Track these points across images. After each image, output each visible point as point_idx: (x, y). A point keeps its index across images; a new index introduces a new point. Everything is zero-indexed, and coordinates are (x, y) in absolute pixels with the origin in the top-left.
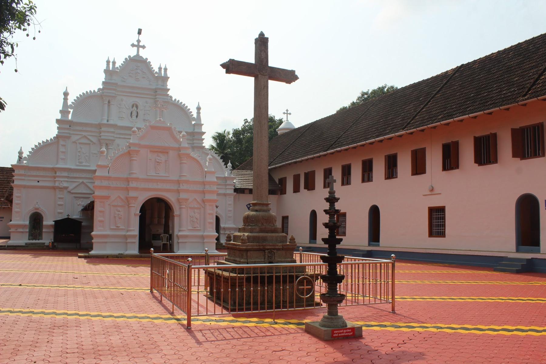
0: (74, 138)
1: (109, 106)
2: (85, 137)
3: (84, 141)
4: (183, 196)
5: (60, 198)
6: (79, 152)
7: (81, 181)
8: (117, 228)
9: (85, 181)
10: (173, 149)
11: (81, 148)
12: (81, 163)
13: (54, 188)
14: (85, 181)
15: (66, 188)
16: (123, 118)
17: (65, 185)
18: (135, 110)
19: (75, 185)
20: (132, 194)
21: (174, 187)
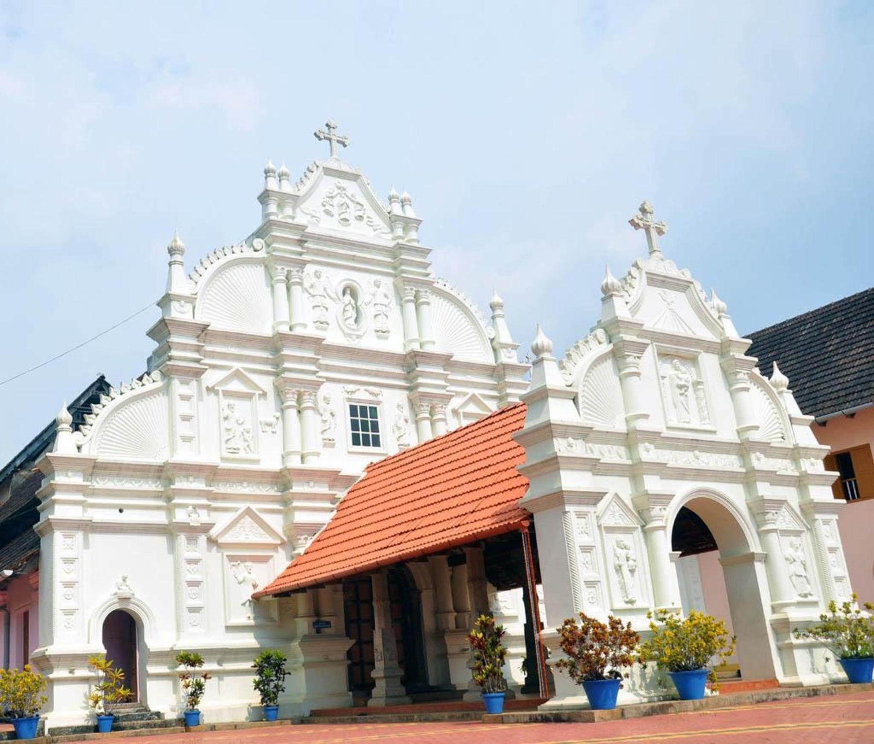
0: (211, 378)
1: (288, 289)
2: (237, 375)
3: (236, 386)
4: (764, 490)
5: (190, 561)
6: (226, 418)
7: (243, 506)
8: (629, 606)
9: (255, 507)
10: (708, 347)
11: (230, 406)
12: (236, 450)
13: (169, 531)
14: (255, 507)
15: (206, 528)
16: (325, 325)
17: (203, 517)
18: (350, 303)
19: (228, 518)
20: (653, 484)
21: (730, 463)
